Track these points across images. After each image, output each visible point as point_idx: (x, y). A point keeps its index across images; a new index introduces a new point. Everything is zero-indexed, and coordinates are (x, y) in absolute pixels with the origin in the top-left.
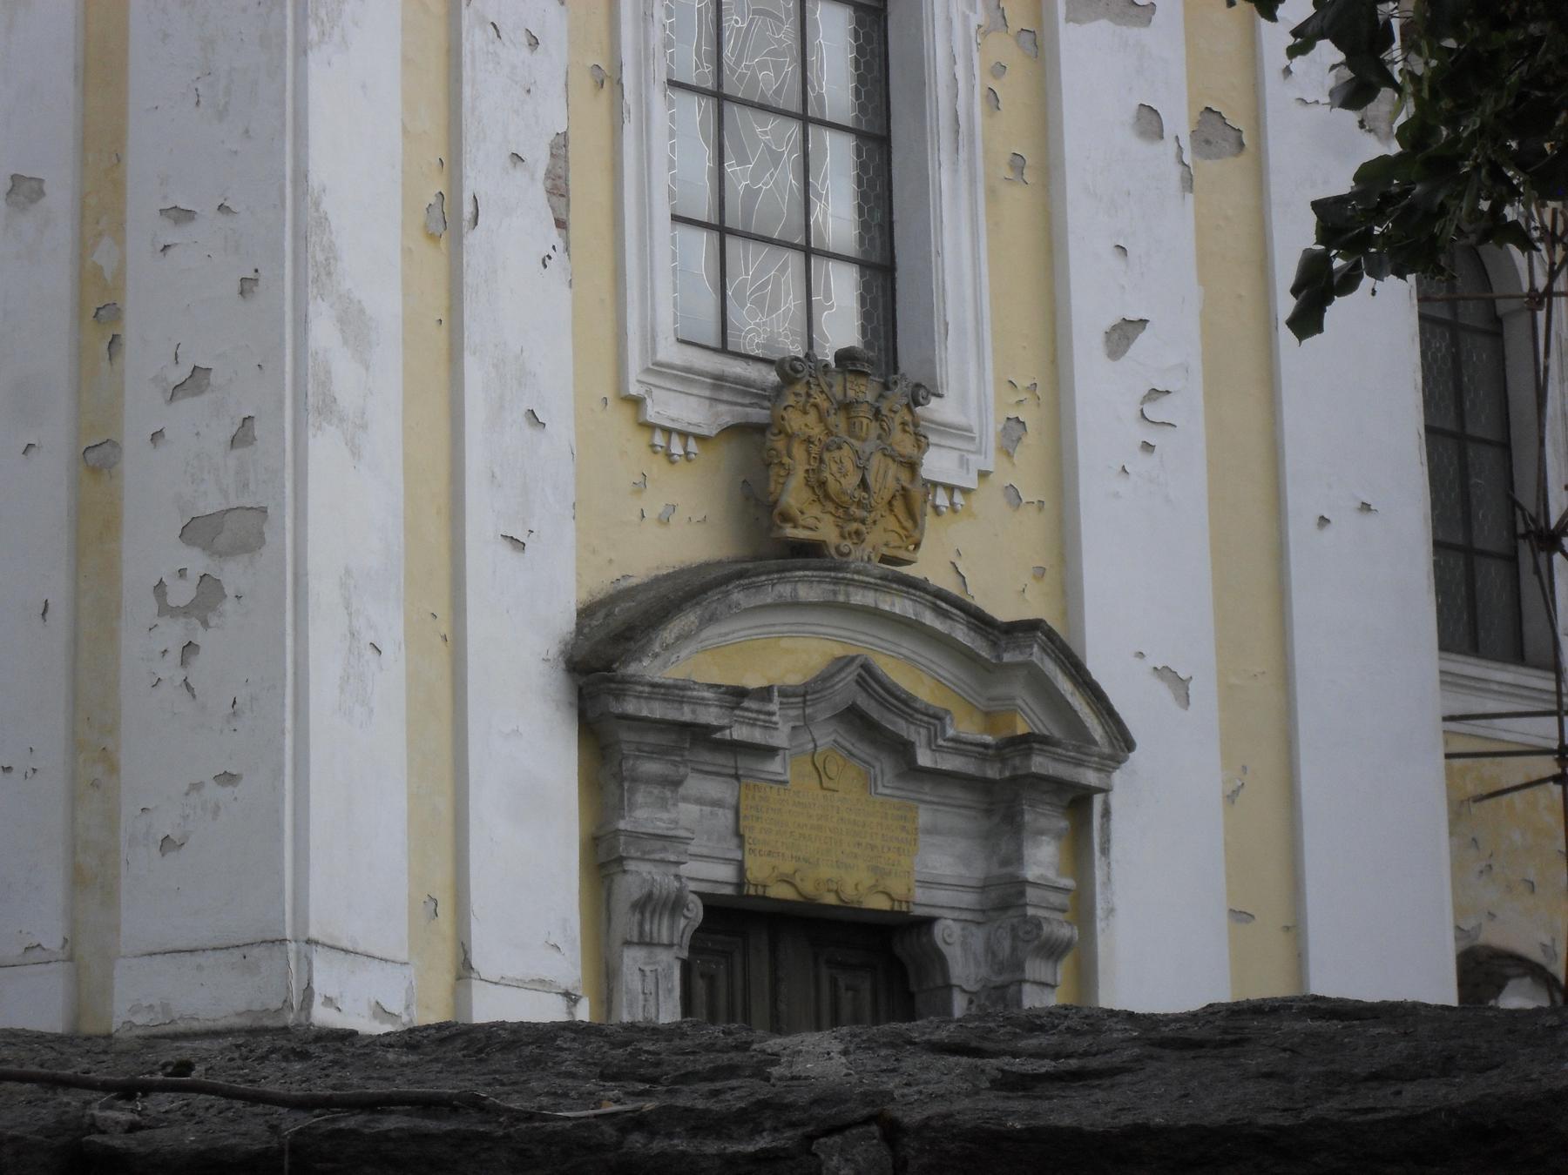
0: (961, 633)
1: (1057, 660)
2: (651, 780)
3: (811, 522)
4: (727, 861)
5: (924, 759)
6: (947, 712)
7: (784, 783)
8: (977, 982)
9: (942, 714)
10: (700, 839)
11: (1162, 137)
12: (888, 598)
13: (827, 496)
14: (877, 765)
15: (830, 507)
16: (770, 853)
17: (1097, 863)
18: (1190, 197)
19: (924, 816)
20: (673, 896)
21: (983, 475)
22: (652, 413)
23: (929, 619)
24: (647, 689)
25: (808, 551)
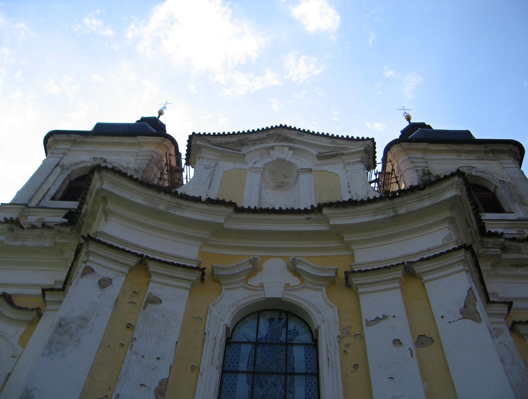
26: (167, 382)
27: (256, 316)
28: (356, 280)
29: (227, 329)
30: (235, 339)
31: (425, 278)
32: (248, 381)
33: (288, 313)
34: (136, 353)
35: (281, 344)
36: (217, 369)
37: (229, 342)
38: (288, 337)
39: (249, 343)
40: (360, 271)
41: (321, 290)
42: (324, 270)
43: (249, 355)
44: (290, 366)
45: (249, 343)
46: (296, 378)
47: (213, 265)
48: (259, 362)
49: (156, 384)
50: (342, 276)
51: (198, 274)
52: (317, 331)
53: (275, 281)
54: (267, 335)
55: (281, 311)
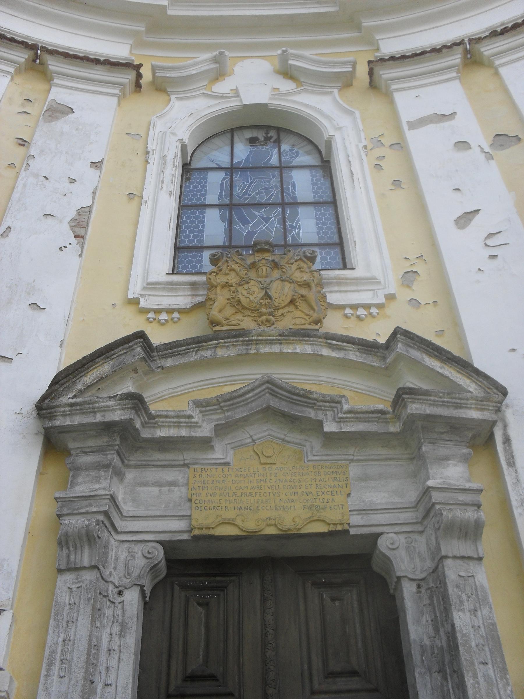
0: (354, 355)
1: (419, 349)
2: (87, 468)
3: (234, 322)
4: (181, 517)
5: (329, 427)
6: (342, 396)
7: (227, 464)
8: (422, 571)
9: (338, 399)
10: (151, 510)
11: (471, 148)
12: (291, 347)
13: (244, 308)
14: (308, 444)
15: (248, 313)
16: (214, 508)
17: (505, 472)
18: (493, 162)
19: (354, 471)
20: (84, 531)
21: (391, 297)
22: (143, 304)
23: (325, 352)
24: (67, 409)
25: (239, 335)
26: (90, 211)
27: (229, 135)
28: (385, 74)
29: (184, 147)
30: (194, 165)
31: (497, 63)
32: (222, 218)
33: (279, 130)
34: (36, 176)
35: (273, 167)
36: (170, 195)
37: (187, 169)
38: (283, 159)
39: (220, 169)
40: (393, 58)
41: (331, 93)
42: (334, 64)
43: (222, 184)
44: (289, 195)
45: (220, 169)
46: (301, 210)
47: (153, 63)
48: (237, 192)
49: (72, 214)
50: (362, 70)
51: (131, 75)
52: (329, 144)
53: (253, 82)
54: (248, 158)
55: (267, 128)
